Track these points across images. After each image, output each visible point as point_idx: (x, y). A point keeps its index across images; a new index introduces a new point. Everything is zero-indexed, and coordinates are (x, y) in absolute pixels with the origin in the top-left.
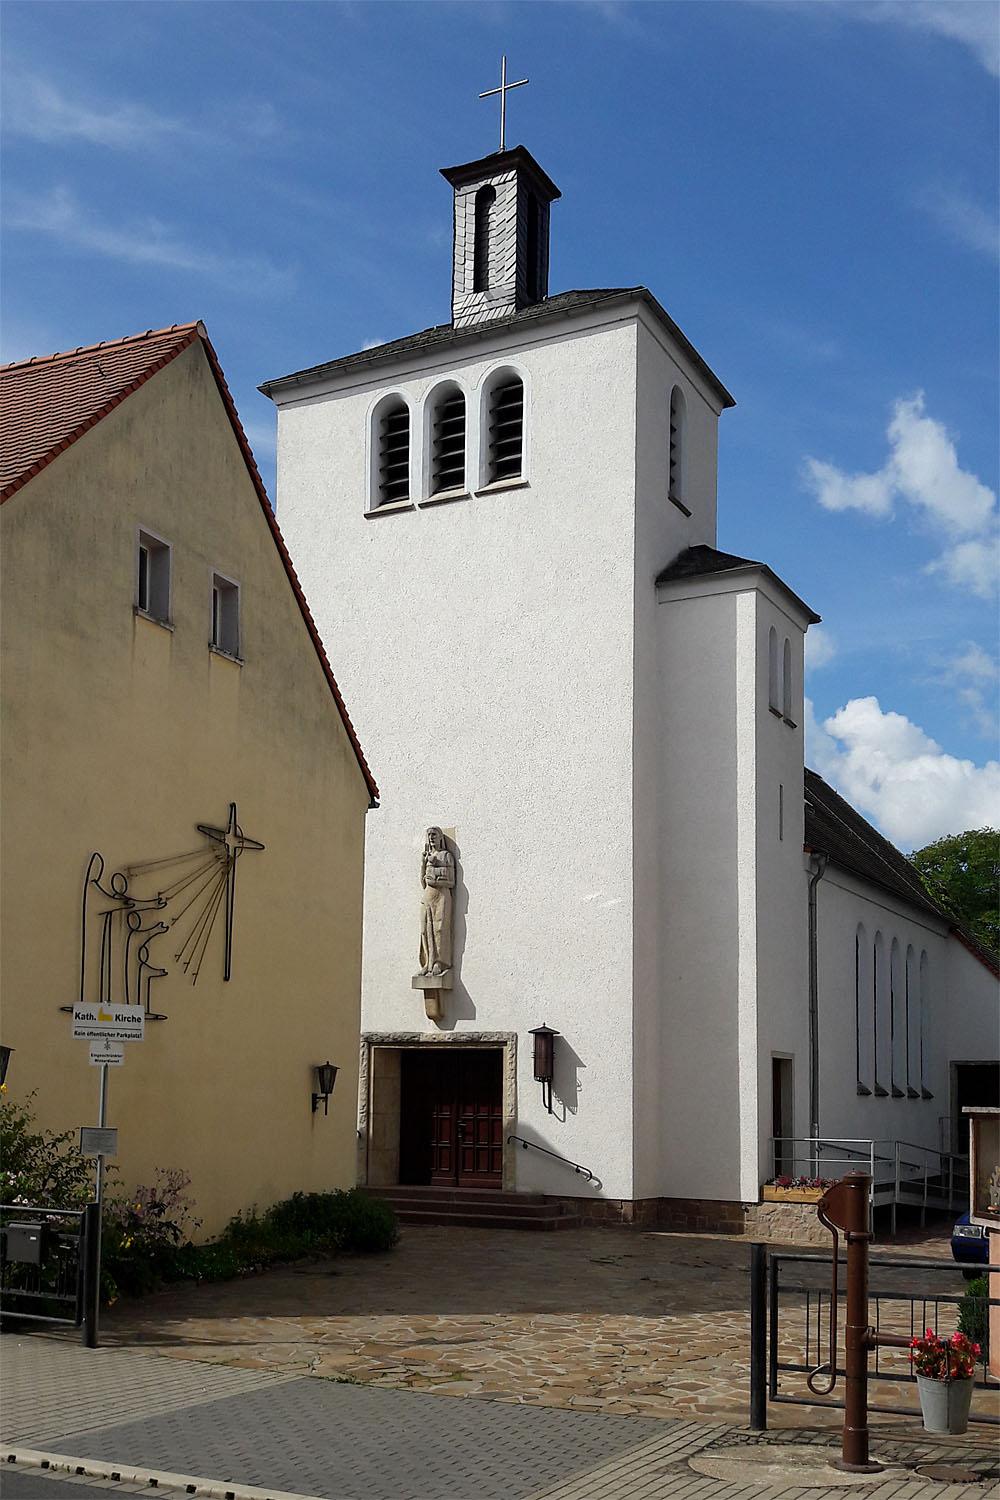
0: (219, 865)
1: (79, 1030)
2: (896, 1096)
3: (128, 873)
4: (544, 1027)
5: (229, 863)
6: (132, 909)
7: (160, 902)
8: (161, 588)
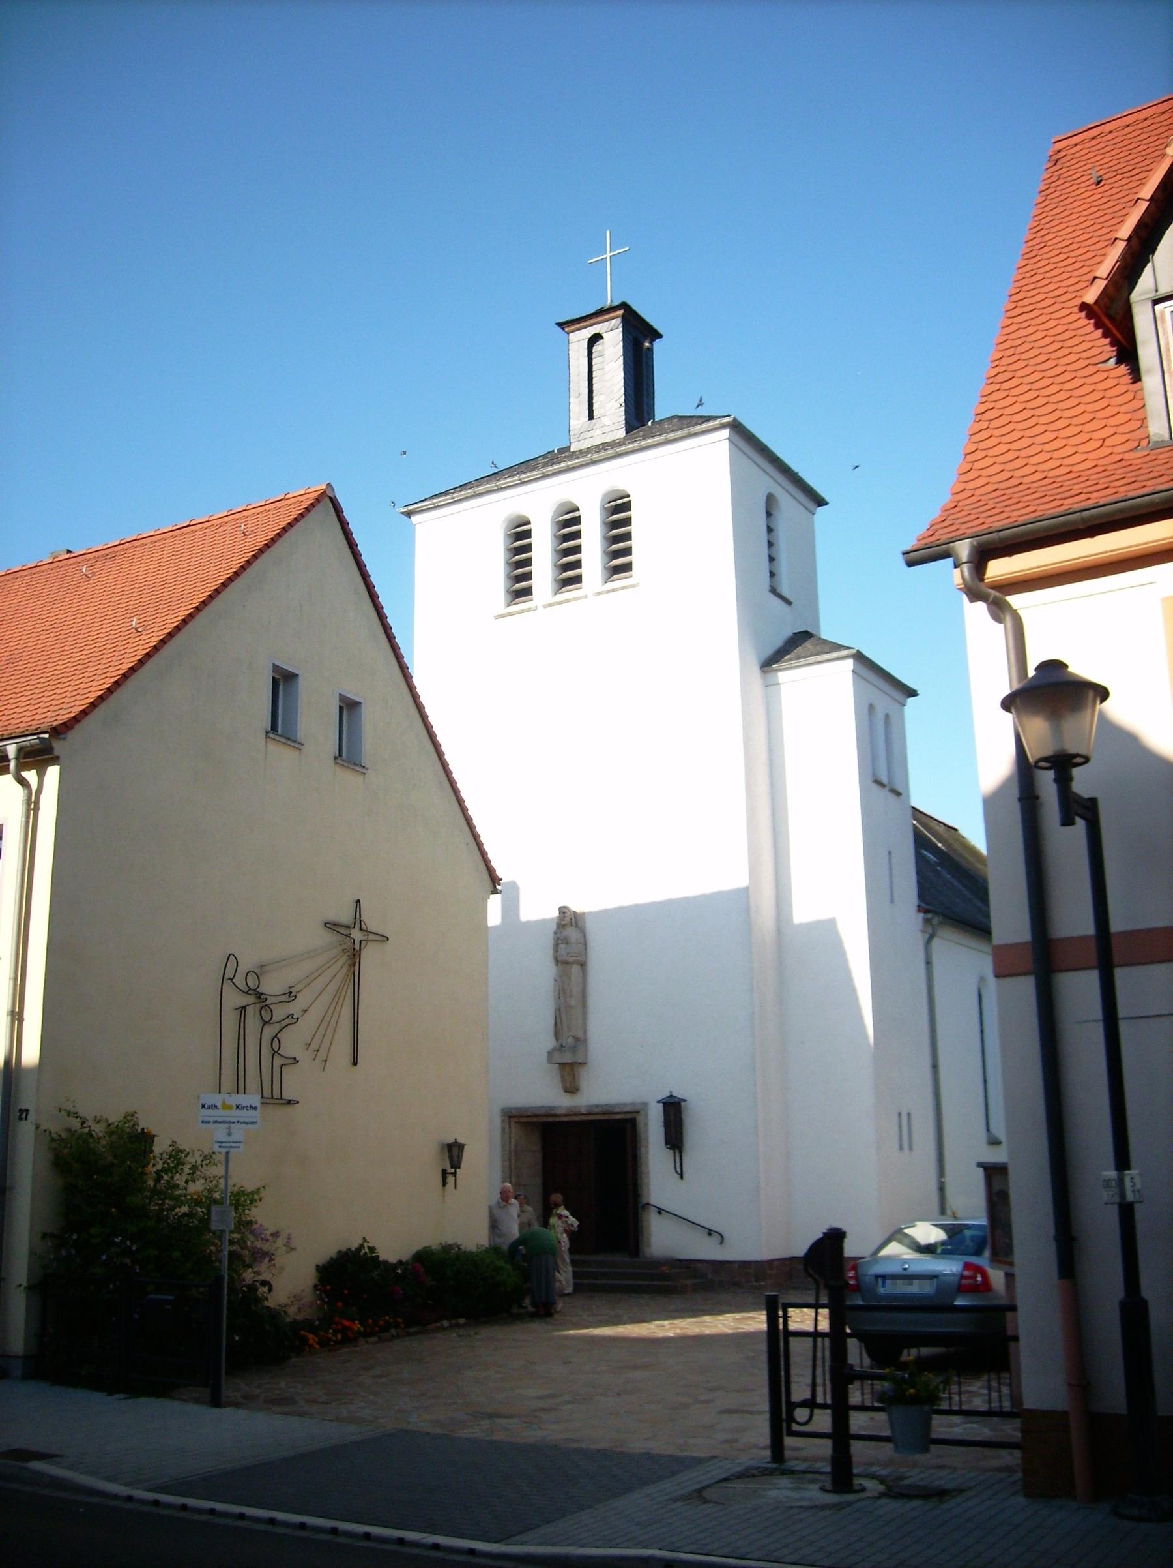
0: (345, 958)
1: (205, 1119)
2: (993, 1144)
3: (258, 973)
4: (671, 1096)
5: (355, 956)
6: (264, 1004)
7: (290, 995)
8: (292, 722)
